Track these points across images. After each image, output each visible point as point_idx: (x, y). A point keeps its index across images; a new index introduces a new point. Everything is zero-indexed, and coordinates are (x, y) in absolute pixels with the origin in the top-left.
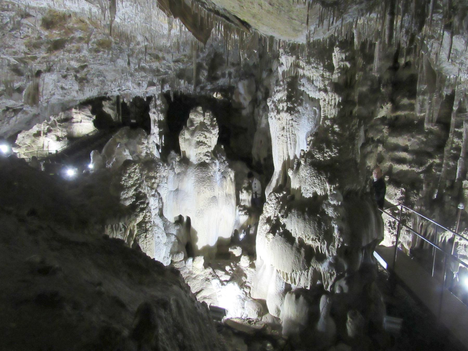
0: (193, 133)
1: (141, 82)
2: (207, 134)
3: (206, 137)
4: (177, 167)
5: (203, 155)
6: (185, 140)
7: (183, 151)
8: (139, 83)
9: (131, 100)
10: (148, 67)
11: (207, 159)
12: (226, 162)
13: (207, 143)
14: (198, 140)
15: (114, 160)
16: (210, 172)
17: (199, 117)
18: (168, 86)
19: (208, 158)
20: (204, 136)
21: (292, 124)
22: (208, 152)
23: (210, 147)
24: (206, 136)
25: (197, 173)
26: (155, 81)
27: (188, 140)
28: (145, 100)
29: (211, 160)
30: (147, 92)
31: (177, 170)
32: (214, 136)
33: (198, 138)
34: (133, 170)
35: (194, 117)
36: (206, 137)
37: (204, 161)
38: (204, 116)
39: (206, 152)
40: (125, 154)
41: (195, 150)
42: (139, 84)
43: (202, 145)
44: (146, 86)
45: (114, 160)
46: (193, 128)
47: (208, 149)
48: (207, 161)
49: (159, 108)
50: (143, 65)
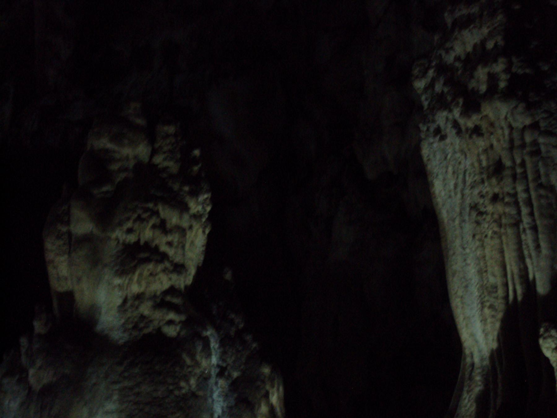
0: (105, 216)
2: (173, 218)
3: (162, 227)
4: (39, 363)
5: (150, 304)
11: (171, 322)
13: (171, 252)
14: (132, 238)
16: (186, 378)
19: (172, 316)
20: (154, 221)
21: (535, 143)
22: (172, 290)
25: (127, 383)
27: (87, 239)
29: (185, 324)
31: (39, 376)
33: (130, 231)
35: (110, 146)
36: (162, 227)
37: (159, 330)
38: (151, 138)
39: (166, 292)
41: (117, 281)
43: (147, 260)
47: (174, 276)
48: (171, 331)
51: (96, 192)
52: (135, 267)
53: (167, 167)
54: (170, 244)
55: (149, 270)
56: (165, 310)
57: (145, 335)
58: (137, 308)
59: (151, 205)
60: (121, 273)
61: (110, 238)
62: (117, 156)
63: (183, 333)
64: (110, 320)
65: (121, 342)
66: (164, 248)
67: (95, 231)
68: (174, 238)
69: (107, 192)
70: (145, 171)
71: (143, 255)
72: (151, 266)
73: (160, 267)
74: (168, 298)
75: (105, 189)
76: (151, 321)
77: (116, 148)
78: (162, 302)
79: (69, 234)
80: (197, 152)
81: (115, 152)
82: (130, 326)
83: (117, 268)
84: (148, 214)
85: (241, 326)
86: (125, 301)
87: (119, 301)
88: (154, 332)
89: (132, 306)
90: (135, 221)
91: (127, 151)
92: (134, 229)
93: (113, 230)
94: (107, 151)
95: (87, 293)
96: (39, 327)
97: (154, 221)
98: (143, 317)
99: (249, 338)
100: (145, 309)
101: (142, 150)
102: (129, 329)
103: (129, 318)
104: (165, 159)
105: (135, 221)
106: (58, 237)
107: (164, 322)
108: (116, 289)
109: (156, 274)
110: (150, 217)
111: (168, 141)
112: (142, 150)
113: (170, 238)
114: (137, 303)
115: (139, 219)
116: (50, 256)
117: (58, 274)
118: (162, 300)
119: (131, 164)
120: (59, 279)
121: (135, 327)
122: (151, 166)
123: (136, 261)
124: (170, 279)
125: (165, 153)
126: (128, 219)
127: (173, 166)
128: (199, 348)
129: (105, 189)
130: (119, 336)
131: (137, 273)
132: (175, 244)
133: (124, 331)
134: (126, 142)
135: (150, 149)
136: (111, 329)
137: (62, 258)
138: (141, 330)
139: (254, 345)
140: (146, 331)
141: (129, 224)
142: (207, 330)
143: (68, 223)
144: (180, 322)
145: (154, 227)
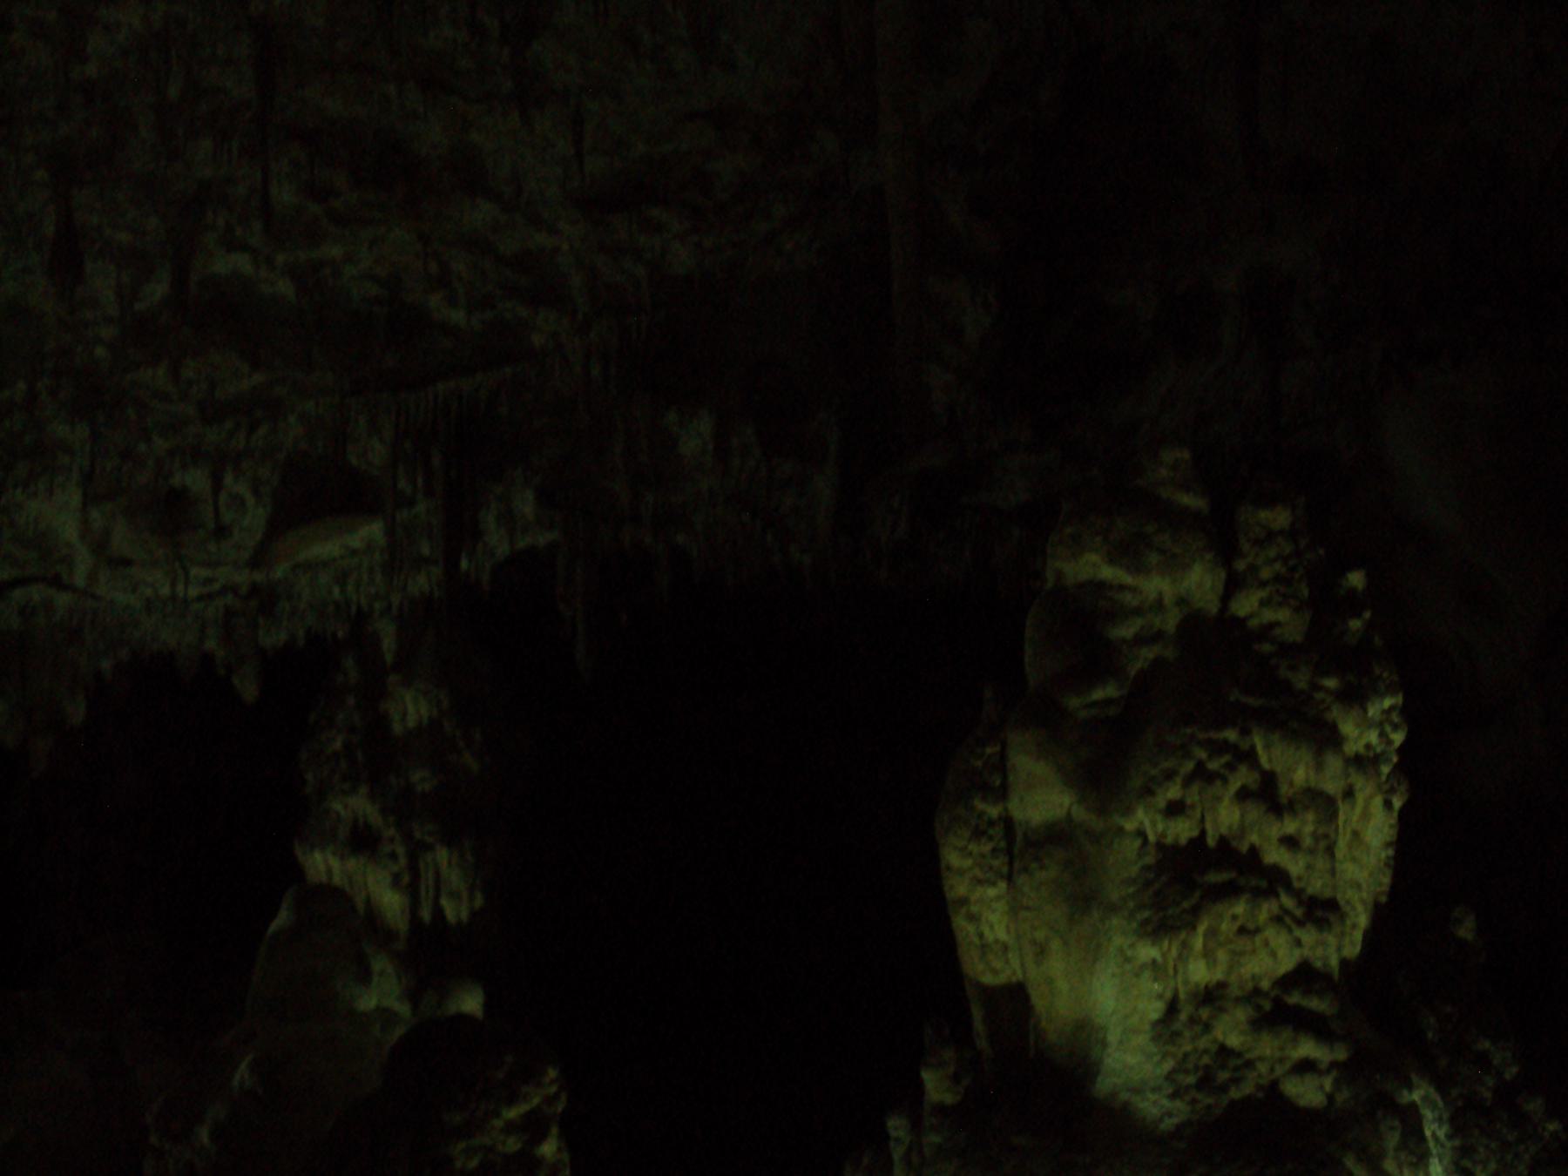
0: (1103, 772)
1: (195, 480)
2: (1296, 768)
3: (1267, 794)
5: (1242, 1014)
6: (1019, 849)
7: (991, 995)
8: (178, 500)
9: (77, 711)
10: (285, 288)
11: (1306, 1067)
12: (1534, 1106)
13: (1295, 866)
14: (1182, 830)
15: (242, 1074)
17: (1174, 564)
18: (526, 503)
19: (1307, 1048)
20: (1243, 777)
22: (1304, 975)
23: (1321, 911)
24: (1269, 782)
26: (371, 452)
27: (1058, 835)
28: (248, 688)
29: (1345, 1072)
30: (266, 600)
32: (1364, 788)
33: (1175, 809)
34: (512, 1145)
35: (1107, 573)
36: (1267, 794)
38: (1226, 551)
39: (1287, 982)
40: (368, 1002)
41: (1148, 952)
42: (170, 514)
44: (255, 518)
45: (242, 1074)
46: (1107, 691)
47: (1308, 936)
48: (1307, 1093)
49: (422, 779)
50: (225, 264)
51: (1073, 702)
52: (1196, 911)
53: (1277, 624)
54: (1291, 842)
55: (1234, 917)
56: (1287, 1033)
57: (1233, 1103)
58: (1207, 1027)
59: (1231, 735)
60: (1158, 930)
61: (1121, 830)
62: (1129, 599)
63: (1343, 1097)
64: (1132, 1064)
65: (1168, 1124)
66: (1274, 856)
67: (1080, 813)
68: (1303, 825)
69: (1108, 702)
70: (1211, 641)
71: (1214, 878)
72: (1240, 908)
73: (1266, 909)
74: (1294, 999)
75: (1098, 694)
76: (1249, 1064)
77: (1128, 579)
78: (1276, 1011)
79: (1008, 823)
80: (1356, 579)
81: (1122, 588)
82: (1191, 1079)
83: (1147, 914)
84: (1226, 758)
85: (1511, 1072)
86: (1172, 1008)
87: (1155, 1010)
88: (1260, 1095)
89: (1192, 1021)
90: (1188, 782)
91: (1156, 585)
92: (1189, 801)
93: (1128, 811)
94: (1100, 586)
95: (1062, 985)
96: (936, 1086)
97: (1243, 777)
98: (1224, 1051)
99: (1534, 1106)
100: (1231, 1030)
101: (1200, 581)
102: (1188, 1088)
103: (1186, 1055)
104: (1264, 603)
105: (1188, 782)
106: (978, 834)
107: (1288, 1065)
108: (1147, 974)
109: (1258, 930)
110: (1231, 767)
111: (1272, 553)
112: (1200, 581)
113: (1290, 826)
114: (1205, 1013)
115: (1202, 775)
116: (957, 888)
117: (981, 936)
118: (1278, 1002)
119: (1171, 621)
120: (984, 948)
121: (1206, 1082)
122: (1228, 623)
123: (1198, 894)
124: (1298, 943)
125: (1263, 584)
126: (1169, 775)
127: (1289, 622)
128: (1392, 1140)
129: (1098, 694)
130: (1159, 1108)
131: (1201, 929)
132: (1308, 841)
133: (1173, 1096)
134: (1154, 558)
135: (1223, 575)
136: (1137, 1091)
137: (992, 892)
138: (1224, 1089)
139: (1552, 1126)
140: (1234, 1094)
141: (1173, 792)
142: (1410, 1088)
143: (1002, 794)
144: (1334, 1065)
145: (1243, 795)
